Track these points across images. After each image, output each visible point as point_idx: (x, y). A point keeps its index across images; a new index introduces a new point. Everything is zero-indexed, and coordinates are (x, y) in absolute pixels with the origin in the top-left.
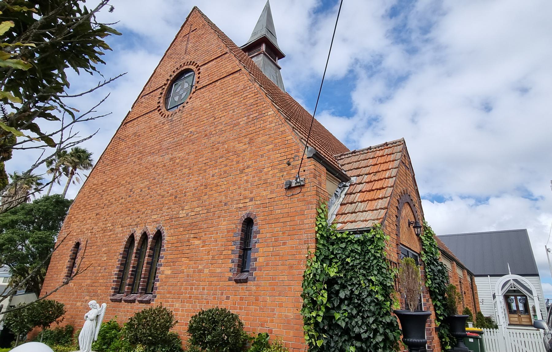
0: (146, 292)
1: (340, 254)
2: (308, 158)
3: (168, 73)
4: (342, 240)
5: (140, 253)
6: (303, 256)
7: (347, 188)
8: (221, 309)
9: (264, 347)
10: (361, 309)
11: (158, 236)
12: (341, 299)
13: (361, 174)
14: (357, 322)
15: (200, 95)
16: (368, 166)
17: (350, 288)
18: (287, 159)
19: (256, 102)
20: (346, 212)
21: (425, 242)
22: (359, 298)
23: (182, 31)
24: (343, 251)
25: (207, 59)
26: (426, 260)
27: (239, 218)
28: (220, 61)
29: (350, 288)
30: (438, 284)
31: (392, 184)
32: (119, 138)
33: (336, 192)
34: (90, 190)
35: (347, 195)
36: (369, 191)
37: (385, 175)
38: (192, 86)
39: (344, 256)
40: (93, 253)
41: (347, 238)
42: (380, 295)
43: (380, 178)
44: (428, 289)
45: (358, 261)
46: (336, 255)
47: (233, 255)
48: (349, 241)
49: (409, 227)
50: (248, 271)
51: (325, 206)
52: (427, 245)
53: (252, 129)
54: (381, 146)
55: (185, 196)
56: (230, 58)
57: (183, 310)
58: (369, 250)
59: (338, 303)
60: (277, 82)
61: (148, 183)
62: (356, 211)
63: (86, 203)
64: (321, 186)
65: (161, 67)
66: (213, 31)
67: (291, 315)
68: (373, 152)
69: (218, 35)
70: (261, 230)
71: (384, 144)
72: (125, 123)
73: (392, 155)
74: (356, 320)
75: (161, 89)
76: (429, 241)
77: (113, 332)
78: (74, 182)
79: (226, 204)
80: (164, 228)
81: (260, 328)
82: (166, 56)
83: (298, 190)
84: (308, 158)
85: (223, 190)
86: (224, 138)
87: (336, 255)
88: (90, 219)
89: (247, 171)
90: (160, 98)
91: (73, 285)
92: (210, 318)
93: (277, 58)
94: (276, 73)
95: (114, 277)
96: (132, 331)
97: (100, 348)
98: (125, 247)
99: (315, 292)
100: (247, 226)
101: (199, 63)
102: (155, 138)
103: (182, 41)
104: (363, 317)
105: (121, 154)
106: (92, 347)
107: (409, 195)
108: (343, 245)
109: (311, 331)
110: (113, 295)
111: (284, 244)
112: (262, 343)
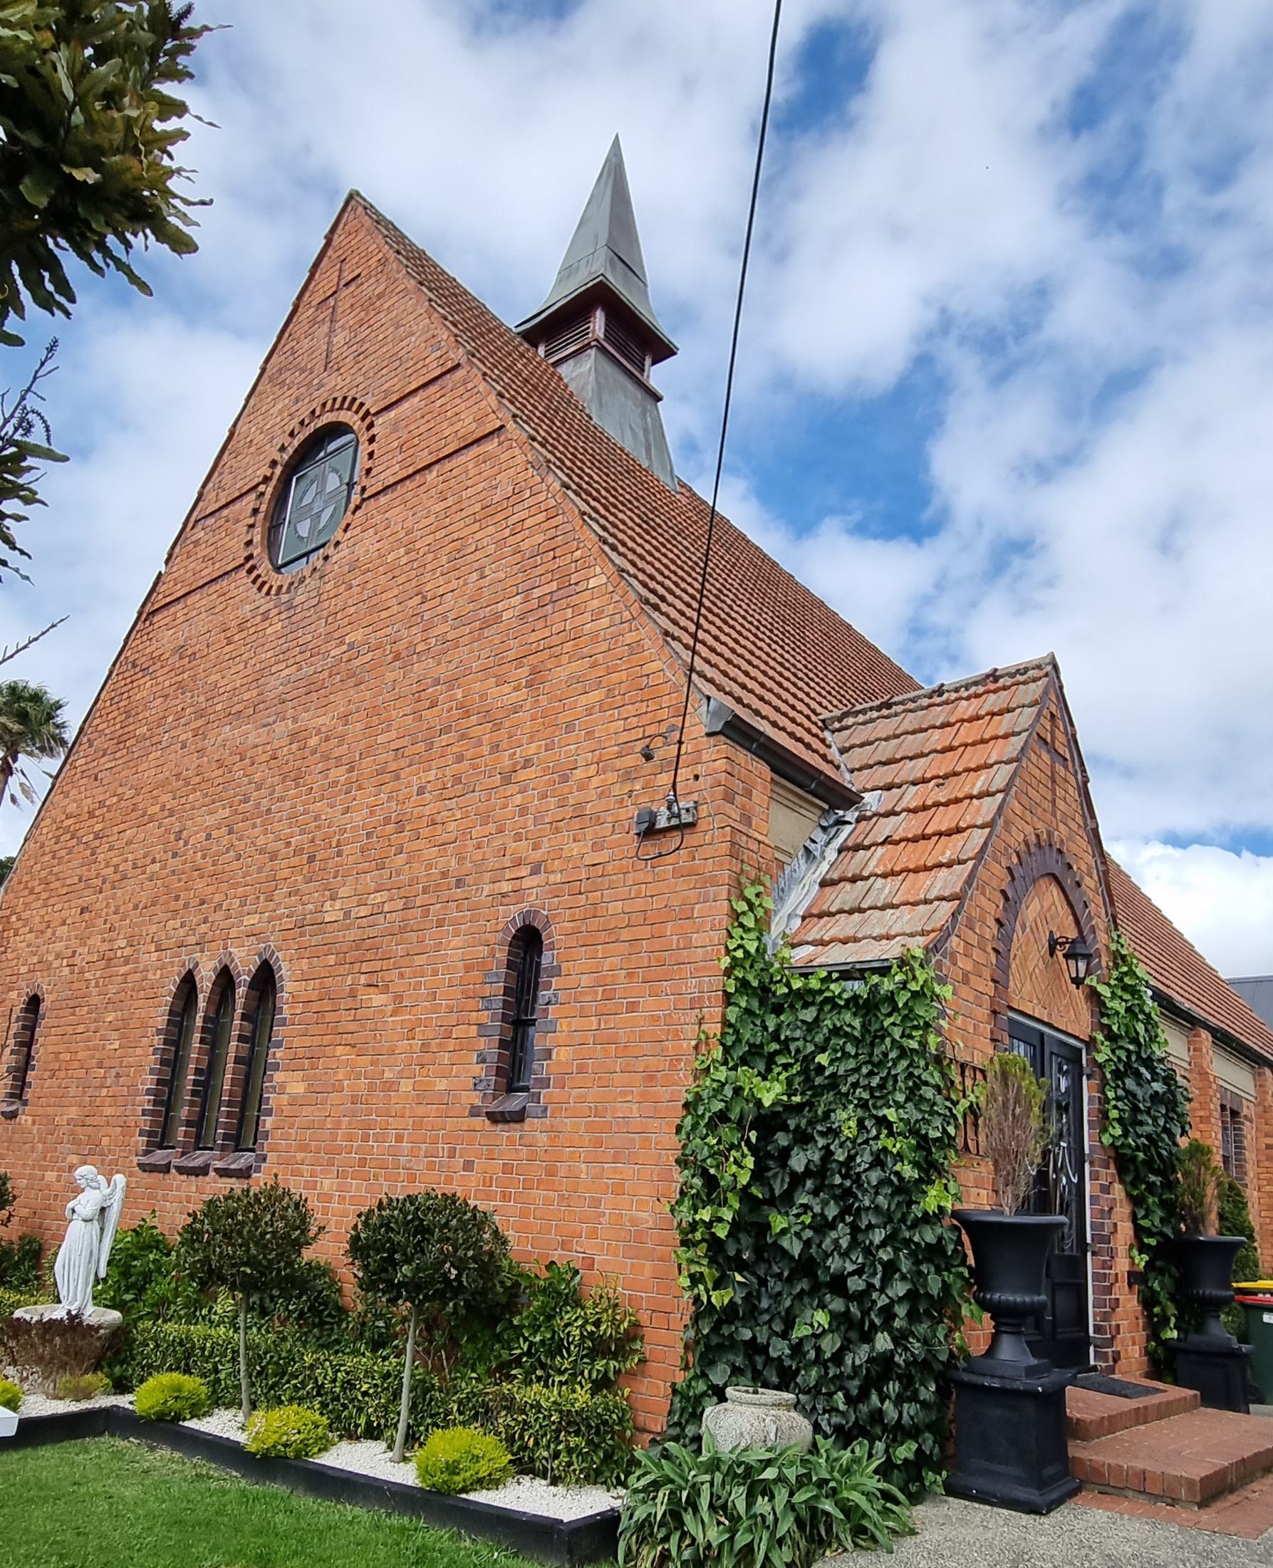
0: (237, 1145)
1: (797, 1039)
2: (709, 735)
3: (273, 438)
4: (804, 998)
5: (216, 1028)
6: (685, 1046)
7: (848, 829)
8: (444, 1194)
9: (566, 1304)
10: (853, 1204)
11: (265, 978)
12: (793, 1174)
13: (897, 781)
14: (836, 1241)
15: (378, 519)
16: (922, 755)
17: (821, 1142)
18: (644, 738)
19: (553, 544)
20: (833, 909)
21: (1109, 1005)
22: (847, 1172)
23: (313, 283)
24: (809, 1030)
25: (396, 388)
26: (1110, 1060)
27: (500, 927)
28: (438, 395)
29: (821, 1142)
30: (1148, 1137)
31: (988, 818)
32: (134, 666)
33: (808, 843)
34: (58, 833)
35: (843, 854)
36: (915, 840)
37: (972, 788)
38: (350, 485)
39: (810, 1048)
40: (81, 1029)
41: (821, 992)
42: (910, 1162)
43: (953, 796)
44: (1112, 1154)
45: (852, 1064)
46: (785, 1044)
47: (482, 1039)
48: (827, 1000)
49: (1052, 953)
50: (526, 1089)
51: (761, 889)
52: (1117, 1013)
53: (538, 635)
54: (976, 683)
55: (339, 854)
56: (470, 386)
57: (344, 1197)
58: (886, 1030)
59: (786, 1186)
60: (648, 449)
61: (227, 812)
62: (864, 905)
63: (51, 873)
64: (750, 825)
65: (252, 417)
66: (413, 282)
67: (646, 1217)
68: (947, 703)
69: (430, 300)
70: (564, 965)
71: (988, 676)
72: (147, 614)
73: (1007, 716)
74: (833, 1235)
75: (253, 496)
76: (1126, 1001)
77: (151, 1257)
78: (13, 799)
79: (459, 883)
80: (280, 954)
81: (560, 1252)
82: (265, 376)
83: (674, 840)
84: (709, 735)
85: (452, 837)
86: (453, 665)
87: (785, 1044)
88: (64, 923)
89: (522, 775)
90: (252, 526)
91: (30, 1122)
92: (410, 1217)
93: (648, 361)
94: (644, 415)
95: (146, 1102)
96: (196, 1251)
97: (118, 1300)
98: (171, 1011)
99: (715, 1153)
100: (525, 953)
101: (372, 404)
102: (242, 665)
103: (313, 322)
104: (855, 1229)
105: (141, 716)
106: (94, 1298)
107: (1060, 851)
108: (809, 1015)
109: (698, 1263)
110: (146, 1153)
111: (632, 1007)
112: (560, 1294)
